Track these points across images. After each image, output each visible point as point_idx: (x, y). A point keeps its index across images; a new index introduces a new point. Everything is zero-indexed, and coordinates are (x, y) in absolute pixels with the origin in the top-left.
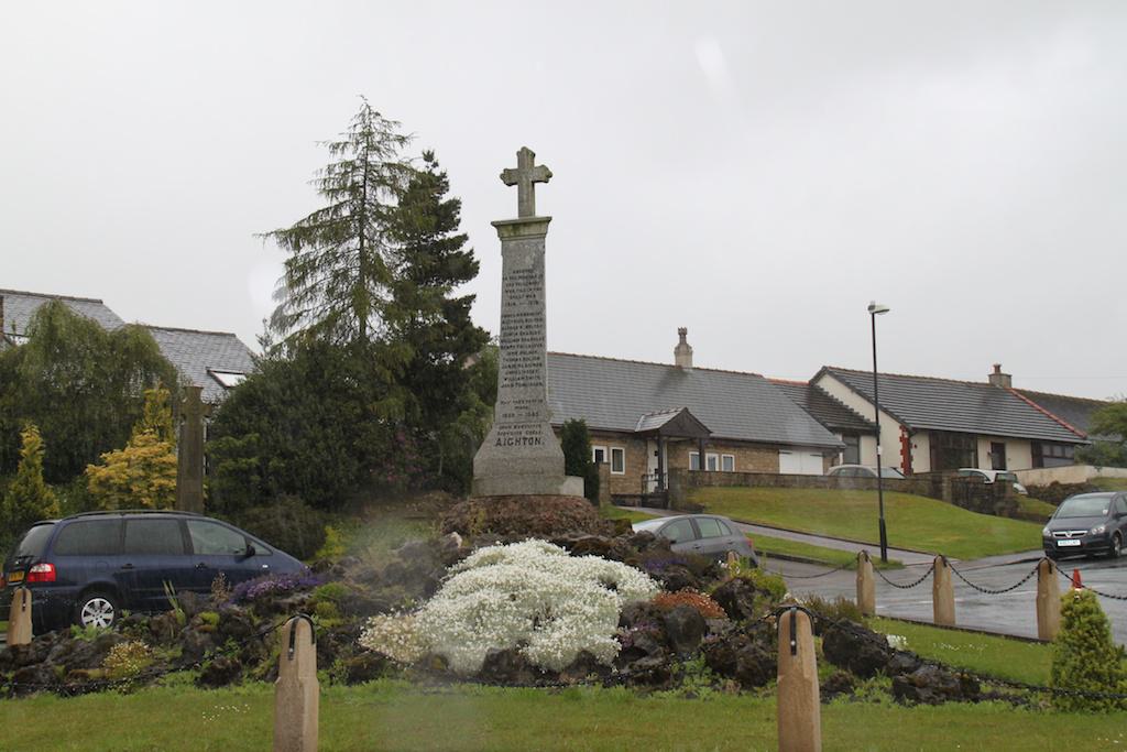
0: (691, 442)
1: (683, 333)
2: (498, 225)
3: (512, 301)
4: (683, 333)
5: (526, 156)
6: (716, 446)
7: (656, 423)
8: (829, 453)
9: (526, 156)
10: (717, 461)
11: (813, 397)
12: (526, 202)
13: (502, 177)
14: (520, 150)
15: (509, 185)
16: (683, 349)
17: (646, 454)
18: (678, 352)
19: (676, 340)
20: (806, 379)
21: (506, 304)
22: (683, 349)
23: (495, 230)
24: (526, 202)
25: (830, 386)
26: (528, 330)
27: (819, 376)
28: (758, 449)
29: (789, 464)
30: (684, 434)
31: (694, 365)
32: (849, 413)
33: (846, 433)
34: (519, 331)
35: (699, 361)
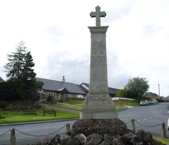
0: (65, 93)
1: (64, 77)
2: (89, 28)
3: (95, 52)
4: (64, 77)
5: (98, 8)
6: (69, 93)
7: (61, 90)
8: (84, 95)
9: (98, 8)
10: (69, 95)
11: (80, 86)
12: (98, 22)
13: (98, 6)
14: (99, 6)
15: (92, 17)
16: (64, 79)
17: (59, 94)
18: (63, 80)
19: (63, 78)
20: (80, 85)
21: (92, 53)
22: (64, 79)
23: (89, 30)
24: (98, 22)
25: (83, 86)
26: (101, 62)
27: (82, 84)
28: (74, 94)
29: (79, 96)
30: (65, 92)
31: (65, 82)
32: (86, 89)
33: (86, 92)
34: (97, 62)
35: (66, 81)
